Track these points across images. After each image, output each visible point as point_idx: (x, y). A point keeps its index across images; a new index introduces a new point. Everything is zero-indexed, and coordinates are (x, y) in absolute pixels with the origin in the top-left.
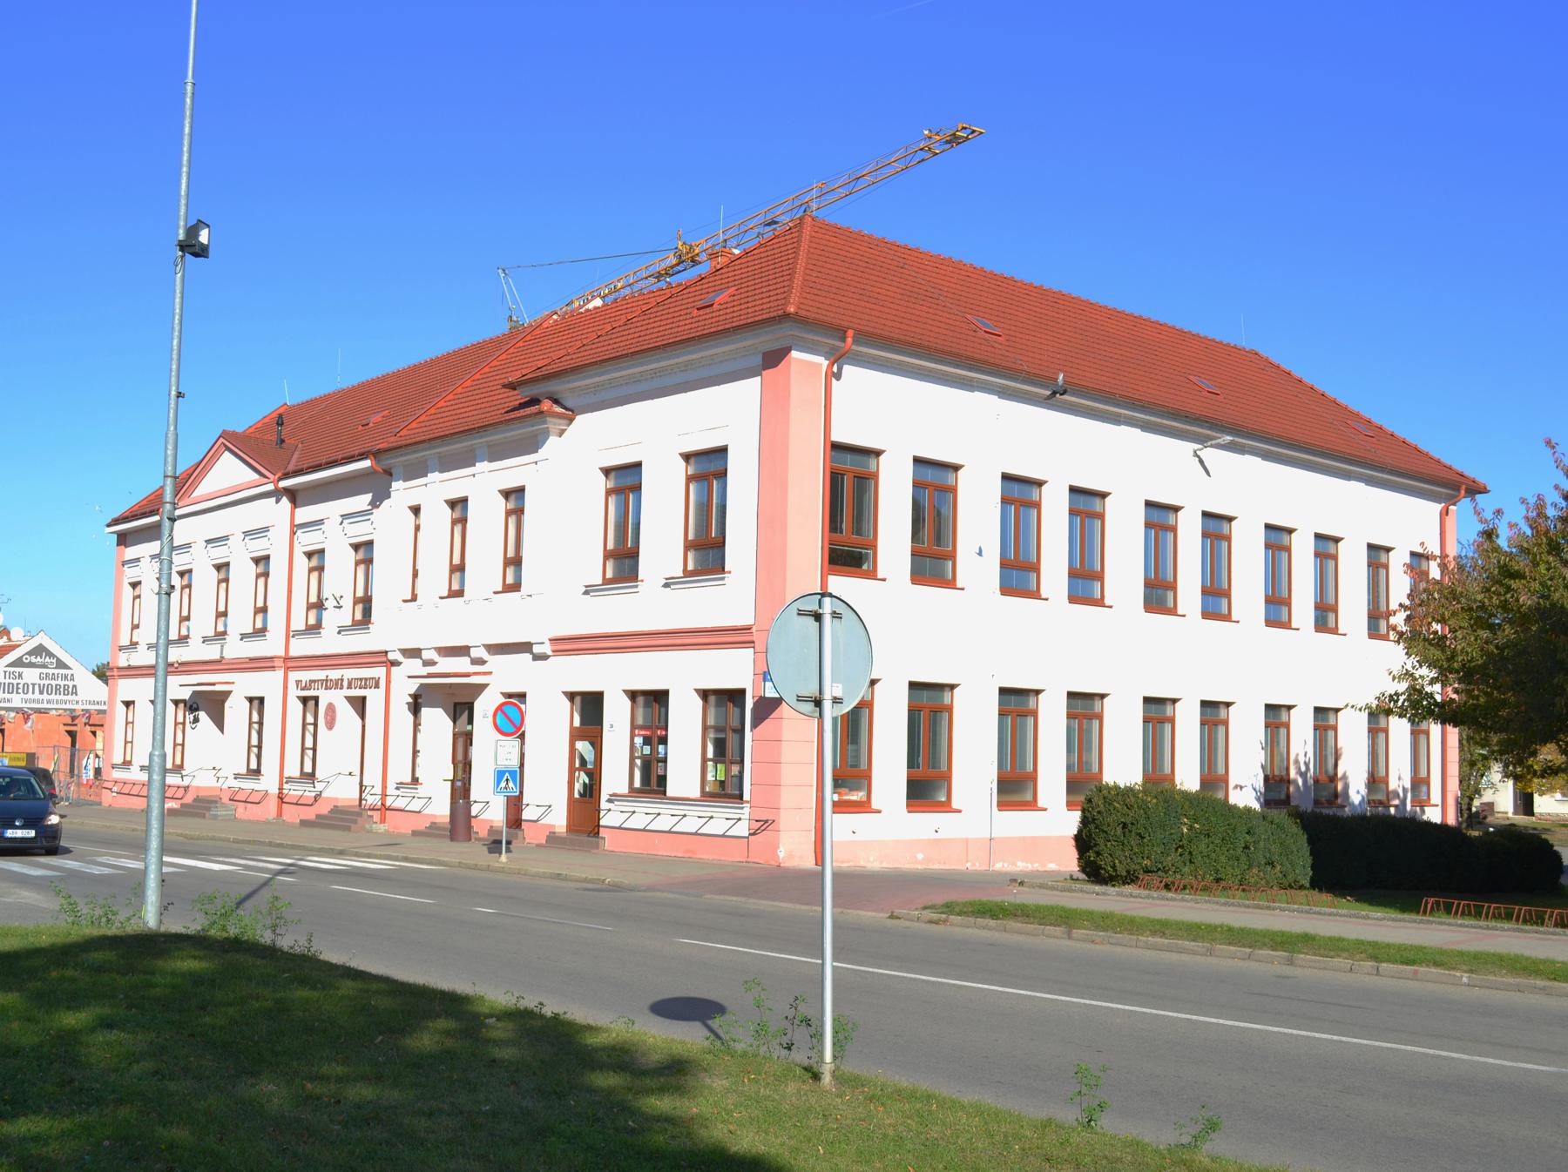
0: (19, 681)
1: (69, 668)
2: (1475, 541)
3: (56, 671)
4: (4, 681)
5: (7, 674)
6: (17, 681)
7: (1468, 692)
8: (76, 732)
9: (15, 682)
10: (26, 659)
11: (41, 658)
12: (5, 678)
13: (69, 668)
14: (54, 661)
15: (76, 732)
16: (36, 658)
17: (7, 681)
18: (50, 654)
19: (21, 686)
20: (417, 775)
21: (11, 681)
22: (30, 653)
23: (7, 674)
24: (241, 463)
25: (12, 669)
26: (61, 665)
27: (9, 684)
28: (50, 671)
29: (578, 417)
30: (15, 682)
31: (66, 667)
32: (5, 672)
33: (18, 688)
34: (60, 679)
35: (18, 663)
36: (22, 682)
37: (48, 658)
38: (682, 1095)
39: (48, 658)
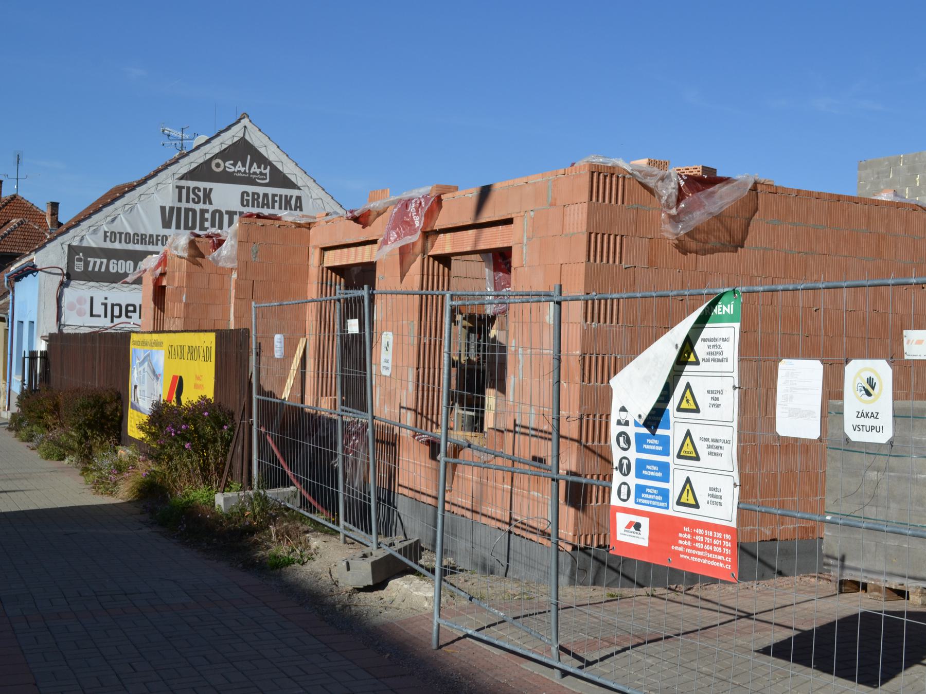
0: (207, 206)
1: (293, 186)
2: (350, 541)
3: (270, 191)
4: (179, 205)
5: (184, 192)
6: (201, 206)
7: (250, 541)
8: (668, 490)
9: (198, 207)
10: (218, 165)
11: (244, 165)
12: (180, 200)
13: (293, 186)
14: (267, 171)
15: (668, 490)
16: (234, 165)
17: (184, 205)
18: (260, 159)
19: (207, 216)
20: (569, 677)
21: (191, 205)
22: (224, 155)
23: (184, 192)
24: (574, 678)
25: (192, 184)
26: (280, 179)
27: (187, 210)
28: (261, 190)
29: (822, 366)
30: (198, 207)
31: (287, 183)
32: (180, 188)
33: (203, 220)
34: (277, 205)
35: (202, 172)
36: (211, 208)
37: (255, 165)
38: (364, 296)
39: (255, 165)
